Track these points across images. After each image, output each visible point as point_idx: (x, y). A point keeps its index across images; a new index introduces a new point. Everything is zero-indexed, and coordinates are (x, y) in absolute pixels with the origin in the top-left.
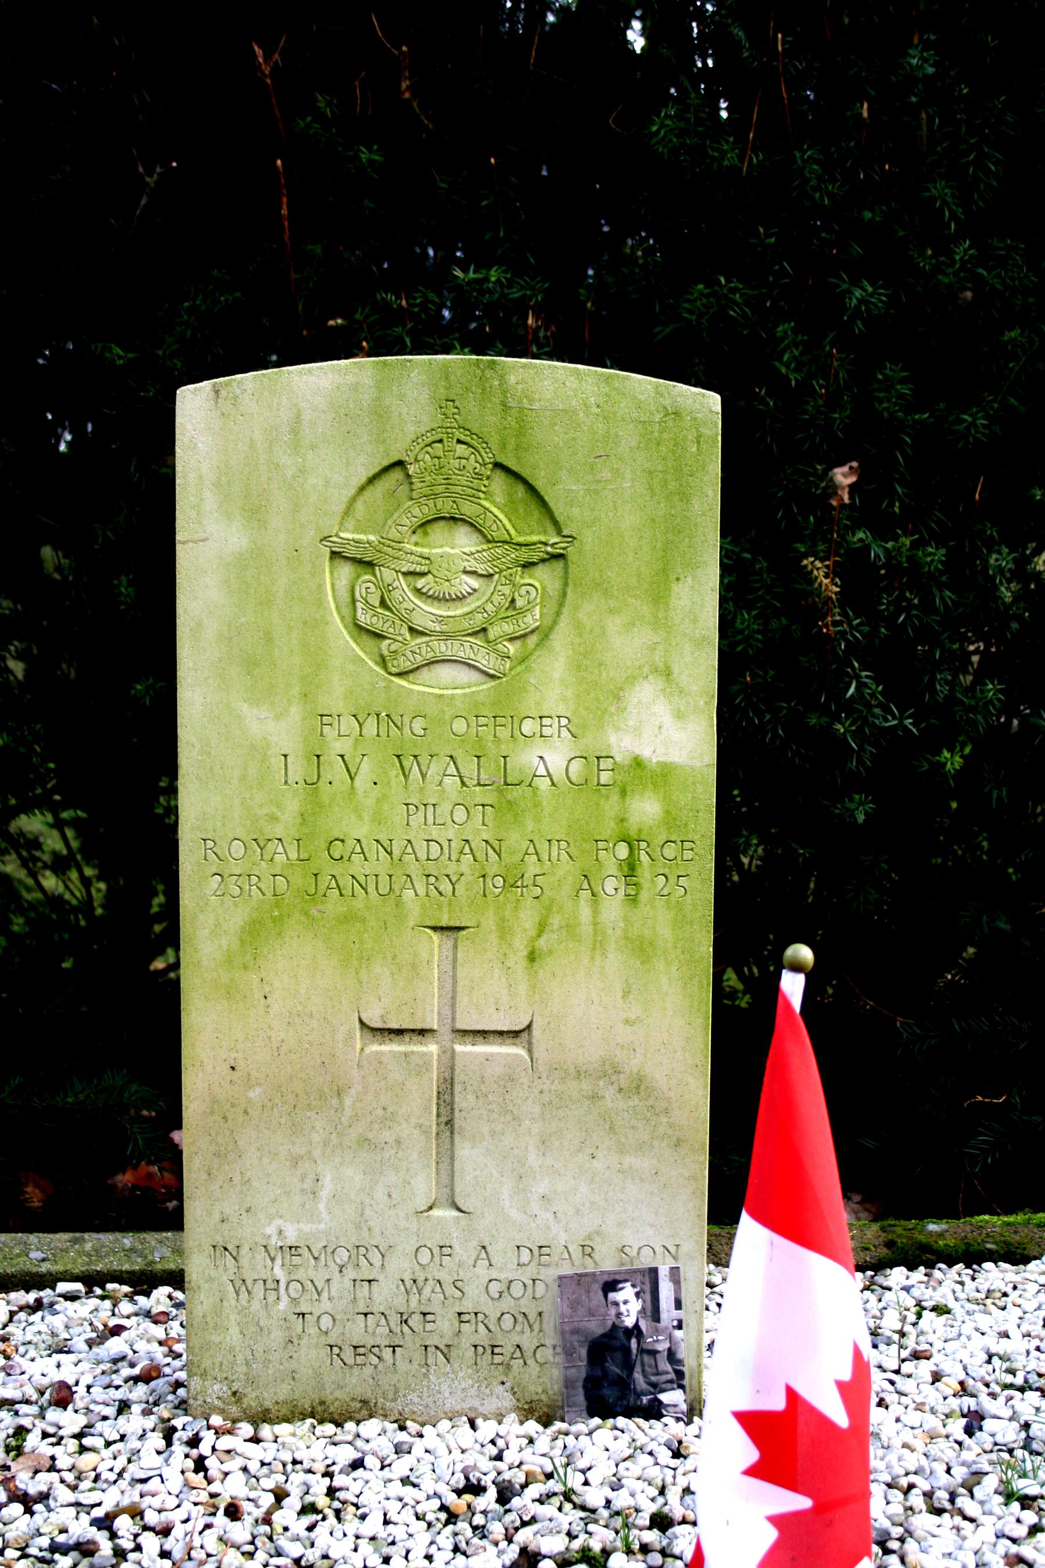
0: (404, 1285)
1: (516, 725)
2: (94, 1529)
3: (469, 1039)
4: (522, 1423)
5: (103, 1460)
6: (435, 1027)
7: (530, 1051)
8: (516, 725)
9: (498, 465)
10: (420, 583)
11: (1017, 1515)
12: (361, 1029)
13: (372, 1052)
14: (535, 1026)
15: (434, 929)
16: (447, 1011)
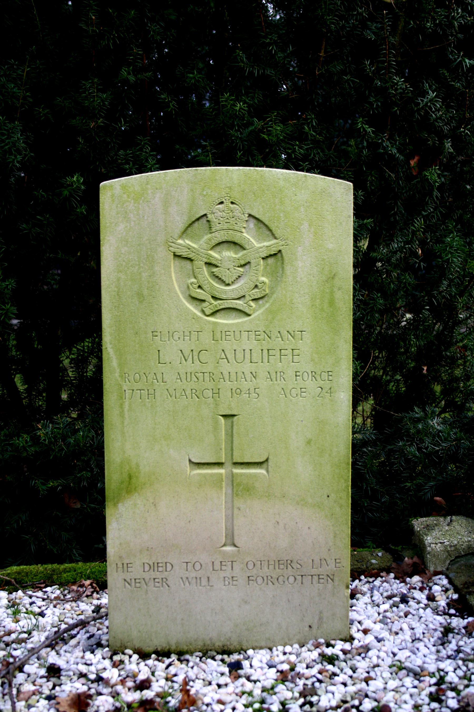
0: (329, 577)
1: (196, 357)
2: (138, 692)
3: (239, 466)
4: (101, 603)
5: (237, 687)
6: (223, 461)
7: (268, 471)
8: (196, 357)
9: (250, 215)
10: (215, 270)
11: (377, 654)
12: (190, 463)
13: (194, 474)
14: (269, 461)
15: (223, 416)
16: (229, 455)
